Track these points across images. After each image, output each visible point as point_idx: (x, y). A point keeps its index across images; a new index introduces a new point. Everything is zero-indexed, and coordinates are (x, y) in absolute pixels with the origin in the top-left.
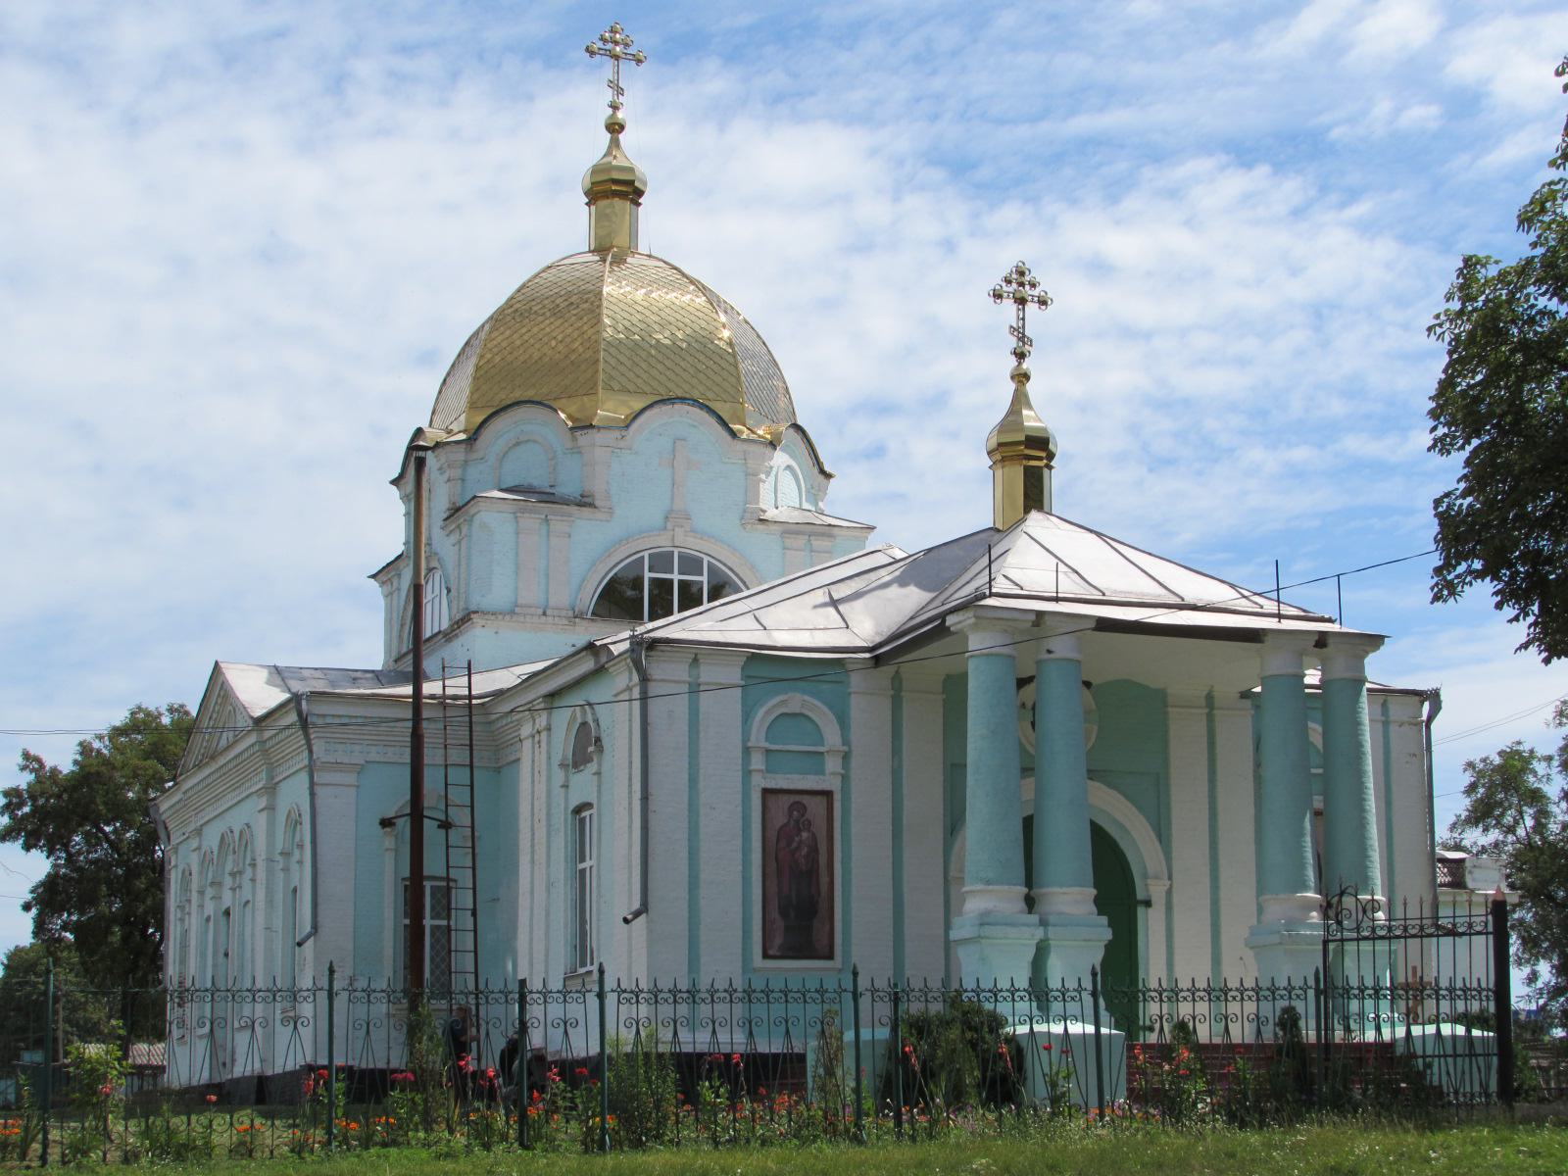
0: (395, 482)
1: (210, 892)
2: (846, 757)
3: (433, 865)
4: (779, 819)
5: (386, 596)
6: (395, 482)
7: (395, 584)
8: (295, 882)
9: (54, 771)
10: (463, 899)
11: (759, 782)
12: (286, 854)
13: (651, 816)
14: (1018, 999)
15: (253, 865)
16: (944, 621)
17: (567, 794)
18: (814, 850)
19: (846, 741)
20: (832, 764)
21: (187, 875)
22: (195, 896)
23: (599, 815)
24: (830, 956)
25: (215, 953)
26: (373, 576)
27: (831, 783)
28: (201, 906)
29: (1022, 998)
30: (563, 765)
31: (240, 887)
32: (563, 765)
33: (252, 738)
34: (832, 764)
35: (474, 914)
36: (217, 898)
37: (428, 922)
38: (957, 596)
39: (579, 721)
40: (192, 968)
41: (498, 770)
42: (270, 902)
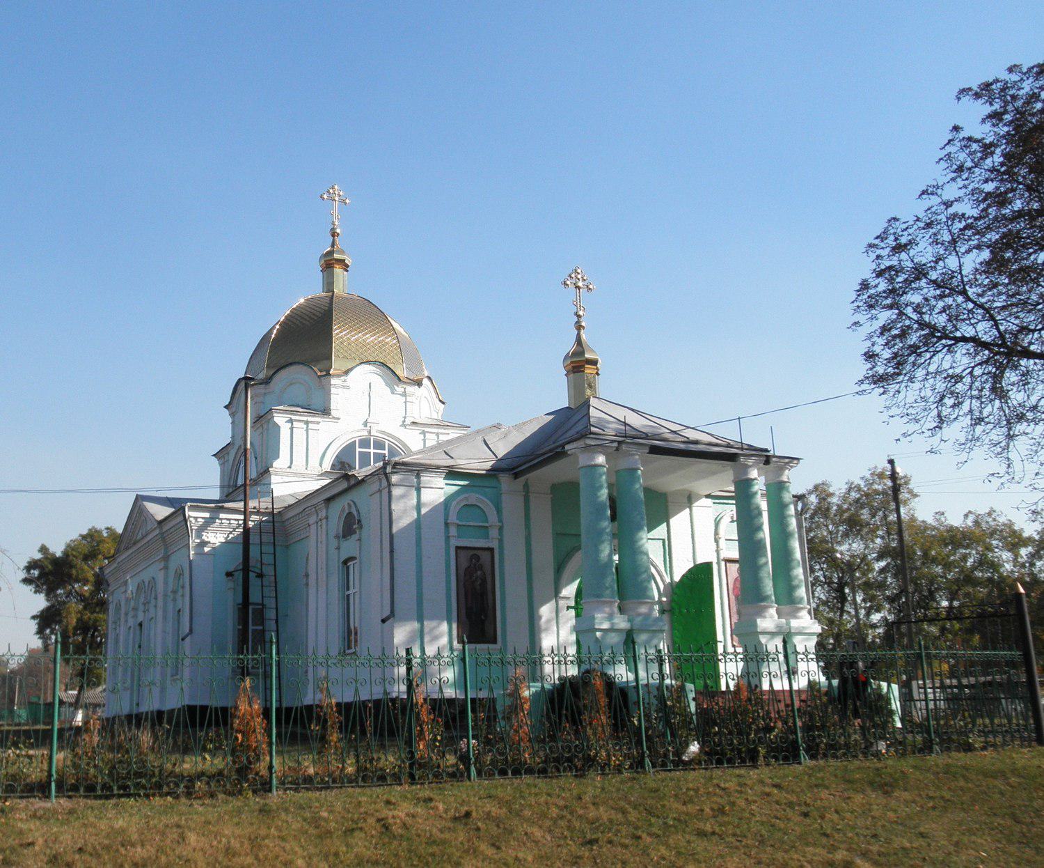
0: (226, 407)
1: (131, 614)
2: (501, 529)
3: (255, 596)
4: (464, 564)
5: (221, 465)
6: (226, 407)
7: (226, 458)
8: (180, 606)
9: (54, 555)
10: (270, 614)
11: (454, 543)
12: (175, 592)
13: (396, 562)
14: (728, 660)
15: (156, 598)
16: (564, 448)
17: (339, 553)
18: (484, 581)
19: (500, 521)
20: (494, 533)
21: (118, 607)
22: (123, 616)
23: (360, 563)
24: (494, 641)
25: (134, 647)
26: (214, 455)
27: (494, 544)
28: (126, 621)
29: (731, 660)
30: (337, 537)
31: (148, 610)
32: (337, 537)
33: (157, 532)
34: (494, 533)
35: (277, 622)
36: (135, 616)
37: (251, 627)
38: (564, 436)
39: (347, 512)
40: (425, 478)
41: (287, 547)
42: (165, 618)
